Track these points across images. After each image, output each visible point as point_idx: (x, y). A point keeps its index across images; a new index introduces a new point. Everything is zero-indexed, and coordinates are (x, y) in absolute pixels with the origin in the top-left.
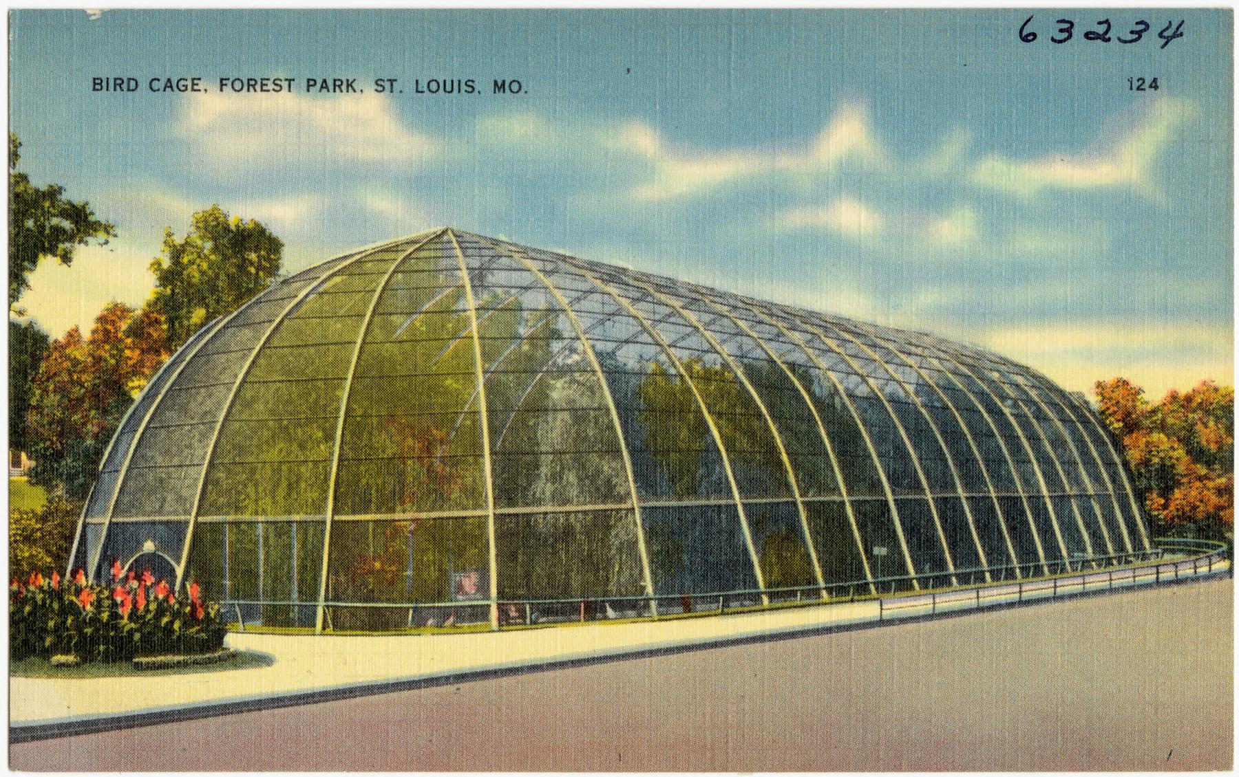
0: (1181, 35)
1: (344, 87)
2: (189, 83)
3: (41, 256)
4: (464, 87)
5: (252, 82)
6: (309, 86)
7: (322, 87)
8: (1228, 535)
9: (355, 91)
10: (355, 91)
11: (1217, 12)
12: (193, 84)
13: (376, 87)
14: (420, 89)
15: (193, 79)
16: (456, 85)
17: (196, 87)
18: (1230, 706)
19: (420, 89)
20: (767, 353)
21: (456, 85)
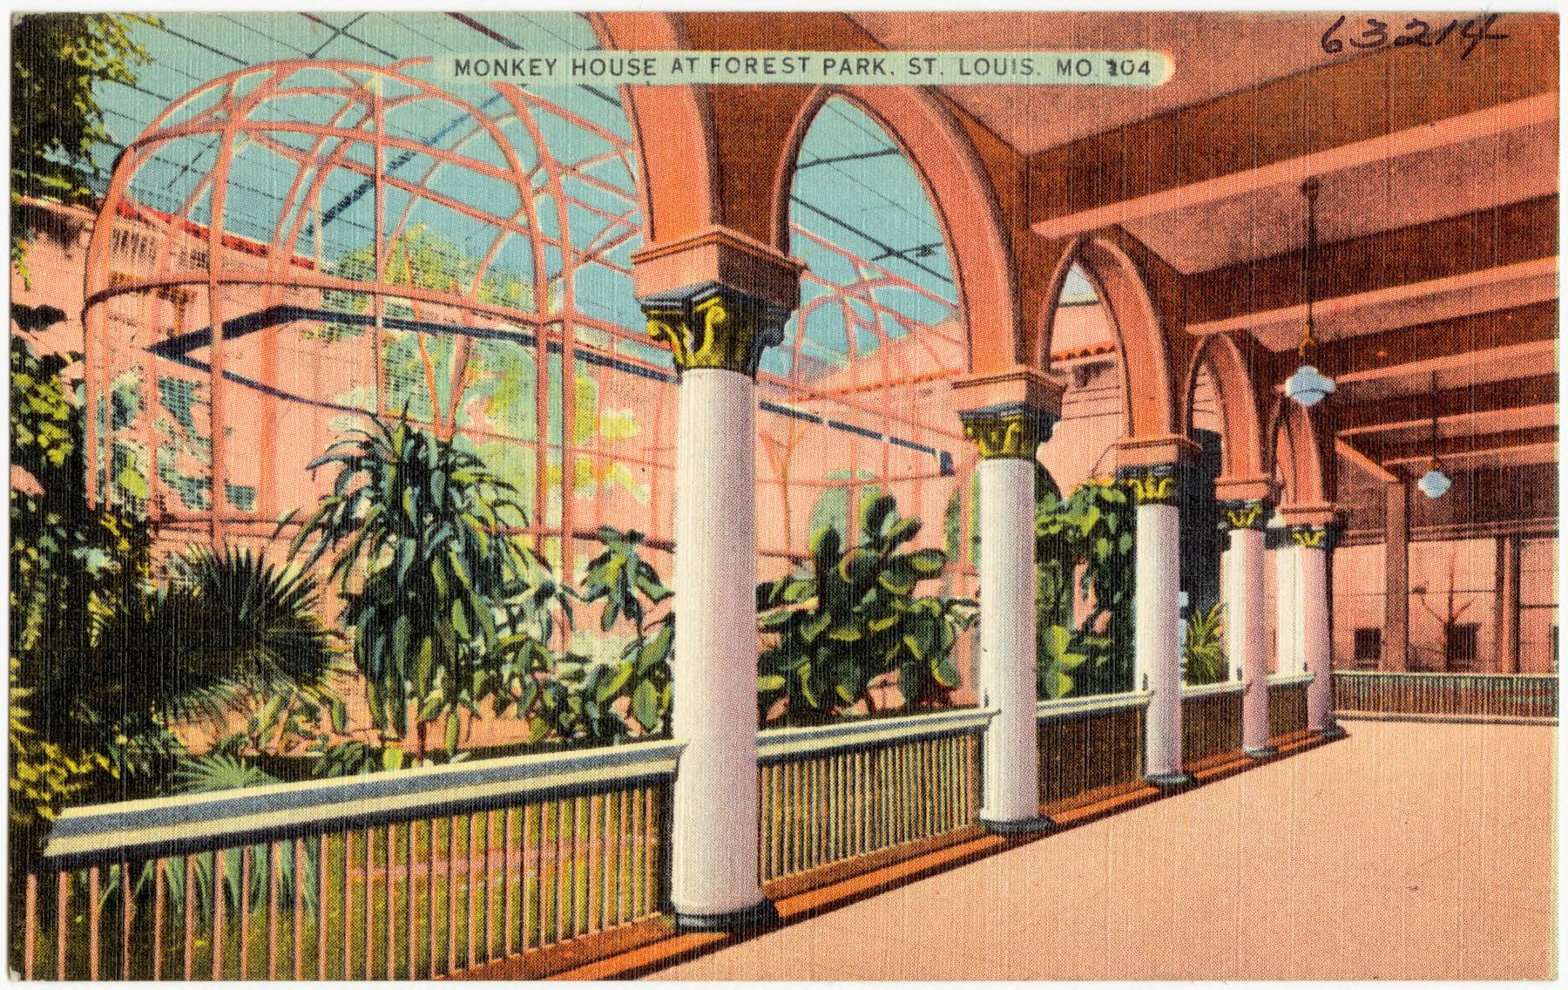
0: (161, 21)
1: (870, 68)
2: (641, 66)
3: (361, 592)
4: (1019, 68)
5: (864, 63)
6: (826, 67)
7: (843, 69)
8: (31, 485)
9: (883, 72)
10: (883, 72)
11: (1537, 17)
12: (647, 67)
13: (1031, 64)
14: (965, 70)
15: (532, 61)
16: (1009, 64)
17: (535, 71)
18: (1540, 863)
19: (965, 70)
20: (196, 365)
21: (1009, 64)
